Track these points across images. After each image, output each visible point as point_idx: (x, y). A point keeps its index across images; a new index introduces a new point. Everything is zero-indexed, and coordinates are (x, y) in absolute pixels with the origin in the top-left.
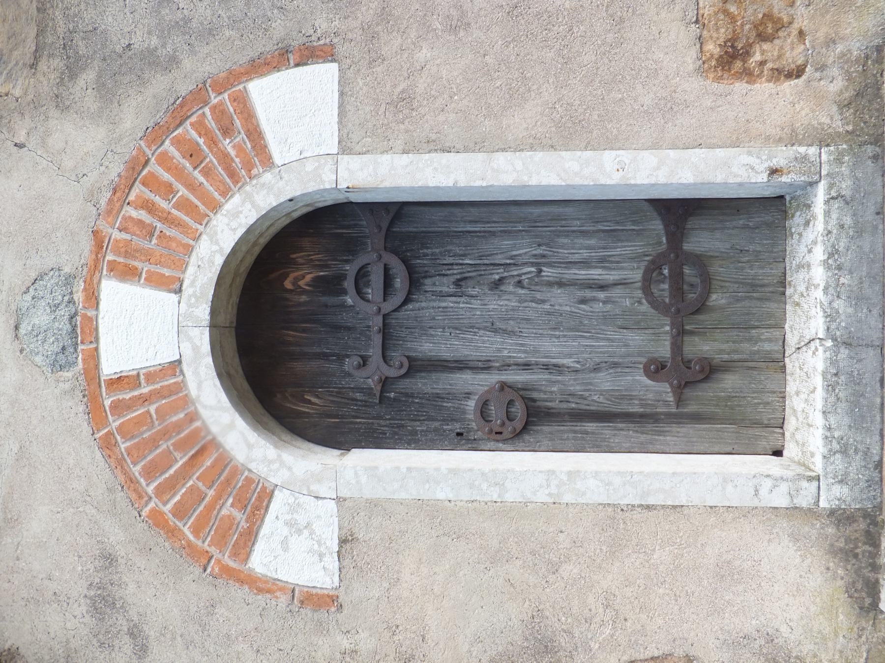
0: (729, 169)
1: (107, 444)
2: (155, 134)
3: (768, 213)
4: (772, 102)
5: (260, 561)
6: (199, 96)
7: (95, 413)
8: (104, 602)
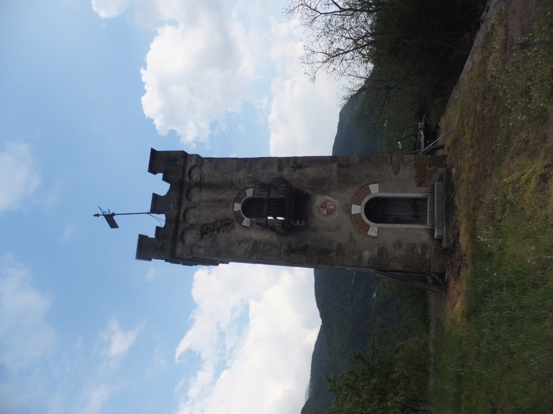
0: (420, 195)
1: (352, 221)
2: (359, 190)
3: (424, 200)
4: (423, 189)
5: (369, 233)
6: (363, 187)
7: (351, 218)
8: (351, 237)
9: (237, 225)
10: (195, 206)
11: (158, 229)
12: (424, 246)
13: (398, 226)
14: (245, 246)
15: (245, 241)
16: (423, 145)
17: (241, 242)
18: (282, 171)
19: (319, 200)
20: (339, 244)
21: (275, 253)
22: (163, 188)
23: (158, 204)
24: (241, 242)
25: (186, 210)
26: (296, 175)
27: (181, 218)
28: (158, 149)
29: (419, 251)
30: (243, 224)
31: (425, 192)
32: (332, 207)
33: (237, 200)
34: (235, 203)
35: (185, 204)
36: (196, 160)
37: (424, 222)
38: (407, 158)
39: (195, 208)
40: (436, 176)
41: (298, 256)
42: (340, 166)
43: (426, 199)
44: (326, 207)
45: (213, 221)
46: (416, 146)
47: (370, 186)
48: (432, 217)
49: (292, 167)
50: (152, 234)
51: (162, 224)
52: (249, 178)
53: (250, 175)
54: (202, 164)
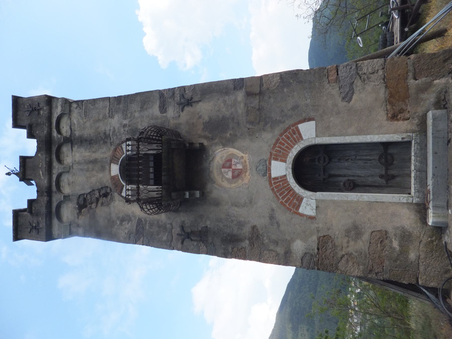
0: (396, 138)
1: (273, 190)
2: (281, 135)
3: (405, 145)
4: (402, 125)
6: (289, 128)
7: (271, 184)
8: (272, 217)
9: (116, 195)
10: (68, 170)
12: (405, 237)
14: (127, 226)
16: (397, 35)
17: (122, 220)
18: (165, 112)
19: (219, 154)
20: (254, 227)
21: (165, 238)
22: (30, 147)
23: (26, 170)
24: (122, 220)
25: (59, 176)
26: (185, 116)
27: (54, 188)
29: (396, 244)
31: (407, 132)
32: (239, 167)
33: (113, 160)
35: (57, 168)
36: (62, 107)
37: (404, 189)
38: (367, 66)
39: (68, 172)
40: (430, 97)
41: (195, 243)
42: (249, 94)
43: (409, 143)
44: (230, 167)
45: (89, 191)
46: (387, 41)
47: (301, 126)
48: (422, 181)
49: (180, 104)
51: (34, 196)
52: (125, 126)
53: (125, 122)
54: (70, 111)
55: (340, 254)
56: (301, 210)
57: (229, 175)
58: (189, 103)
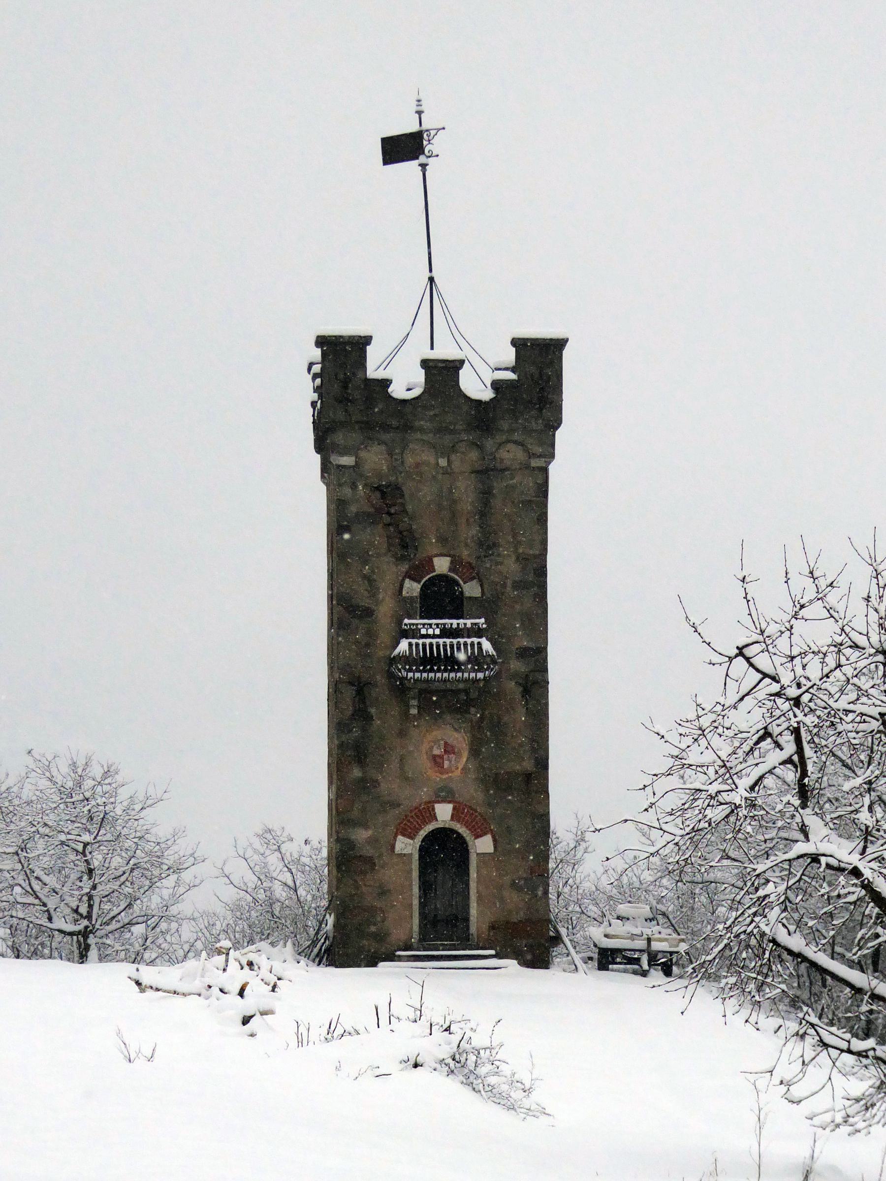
0: (473, 929)
5: (400, 837)
9: (404, 568)
11: (386, 383)
13: (416, 890)
15: (373, 591)
17: (368, 579)
22: (475, 385)
28: (567, 353)
30: (407, 581)
32: (446, 764)
34: (449, 559)
42: (528, 777)
50: (373, 371)
51: (398, 391)
55: (358, 879)
56: (400, 838)
57: (436, 752)
58: (526, 691)
